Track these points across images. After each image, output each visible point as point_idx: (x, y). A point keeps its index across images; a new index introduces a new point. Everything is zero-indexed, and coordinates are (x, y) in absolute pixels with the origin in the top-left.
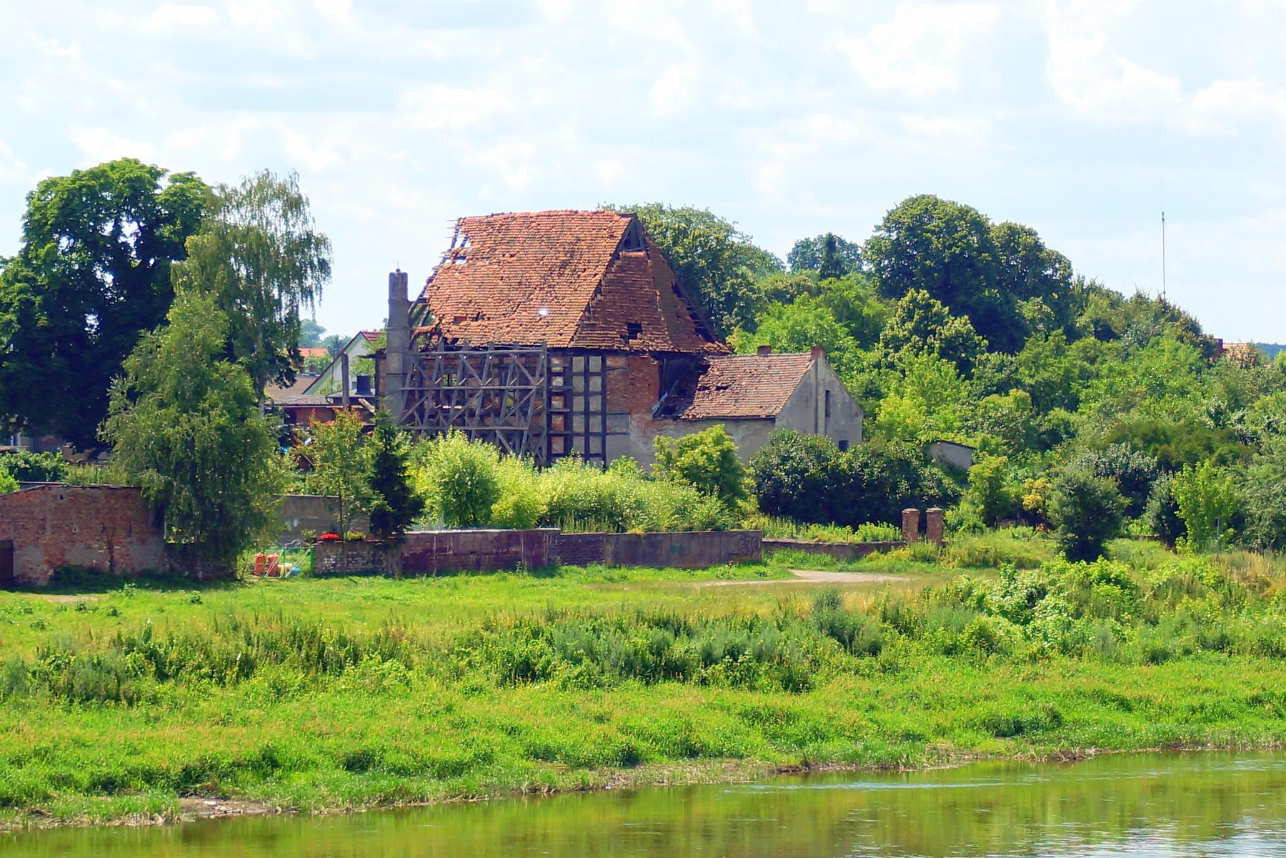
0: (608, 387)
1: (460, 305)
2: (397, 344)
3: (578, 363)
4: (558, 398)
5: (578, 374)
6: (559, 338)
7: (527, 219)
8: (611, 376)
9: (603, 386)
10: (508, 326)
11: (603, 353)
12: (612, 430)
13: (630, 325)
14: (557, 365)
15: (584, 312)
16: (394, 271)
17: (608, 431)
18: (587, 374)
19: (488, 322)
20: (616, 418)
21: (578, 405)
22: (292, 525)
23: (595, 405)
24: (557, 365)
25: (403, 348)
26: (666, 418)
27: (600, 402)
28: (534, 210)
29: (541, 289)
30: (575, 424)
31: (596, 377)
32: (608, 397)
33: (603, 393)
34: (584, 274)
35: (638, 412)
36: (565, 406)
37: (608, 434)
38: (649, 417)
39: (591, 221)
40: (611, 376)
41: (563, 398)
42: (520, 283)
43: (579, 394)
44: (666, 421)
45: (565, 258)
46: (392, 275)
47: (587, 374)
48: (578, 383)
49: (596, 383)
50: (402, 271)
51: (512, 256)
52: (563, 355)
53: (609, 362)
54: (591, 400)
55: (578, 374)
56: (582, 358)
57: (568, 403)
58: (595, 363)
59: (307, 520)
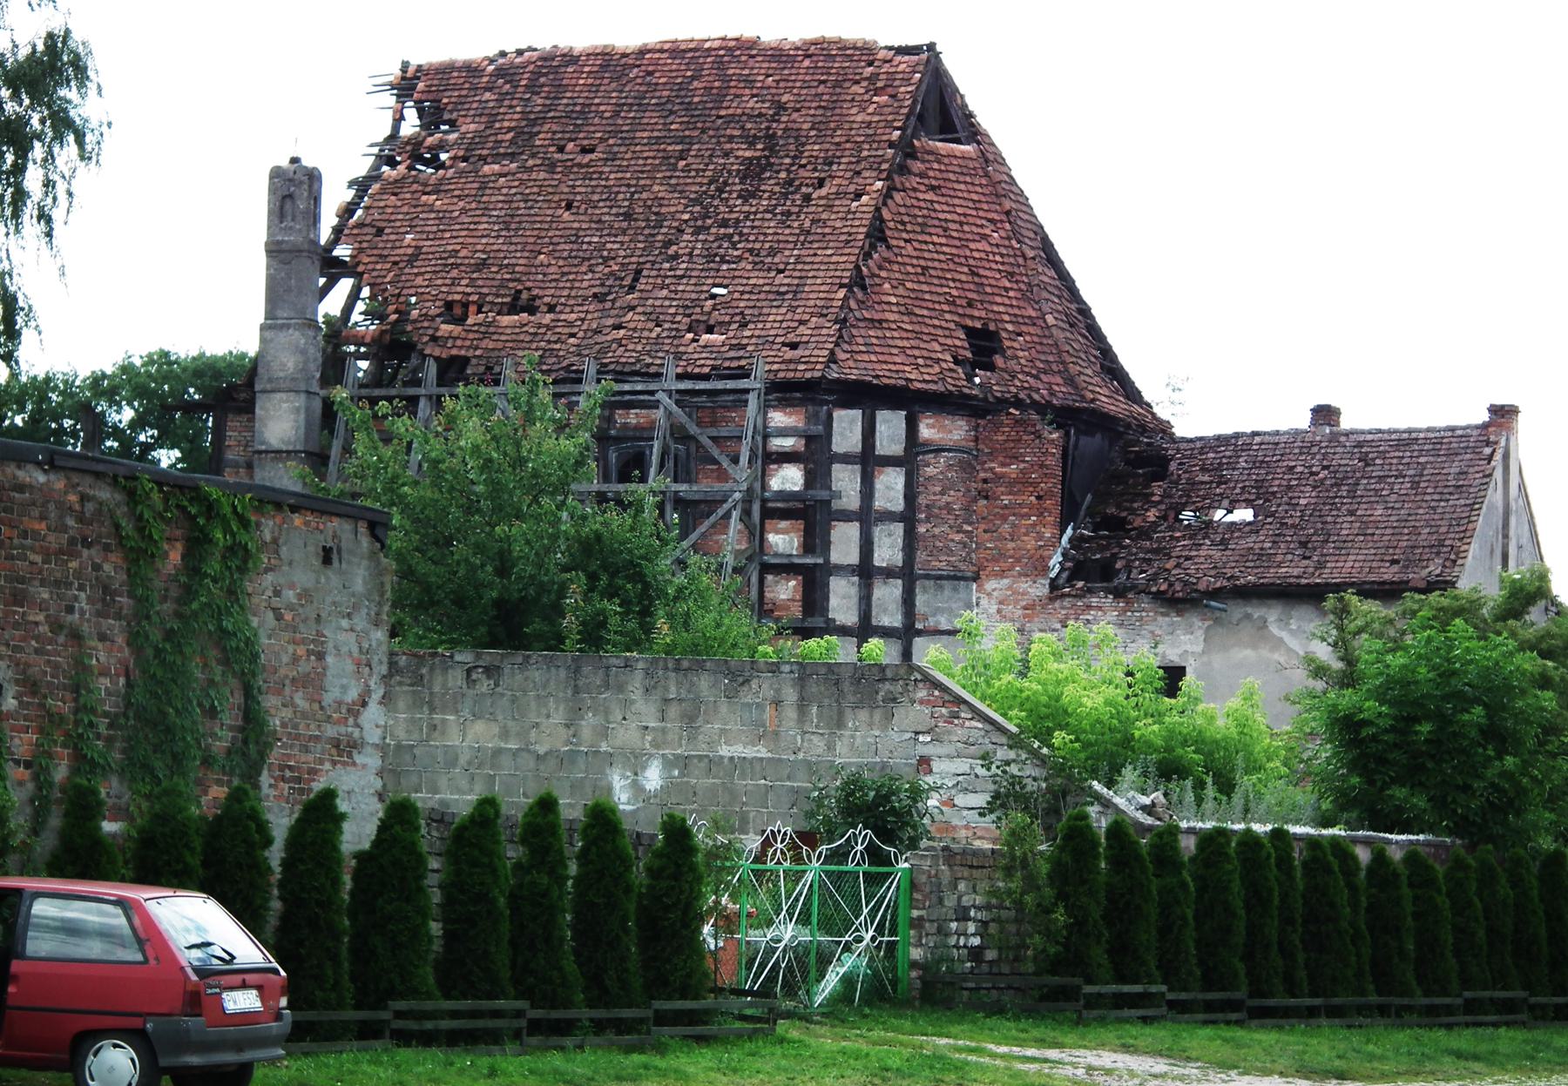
0: (922, 500)
1: (454, 273)
2: (291, 365)
3: (847, 428)
4: (784, 524)
5: (846, 459)
6: (790, 354)
7: (609, 63)
8: (930, 471)
9: (910, 495)
10: (618, 327)
11: (911, 401)
12: (931, 622)
13: (971, 333)
14: (783, 432)
15: (849, 287)
16: (284, 162)
17: (919, 626)
18: (868, 461)
19: (549, 317)
20: (941, 587)
21: (844, 544)
22: (637, 788)
23: (888, 550)
24: (783, 432)
25: (308, 380)
26: (1090, 591)
27: (900, 541)
28: (627, 38)
29: (698, 231)
30: (834, 602)
31: (890, 470)
32: (922, 529)
33: (908, 518)
34: (823, 192)
35: (1002, 574)
36: (808, 548)
37: (920, 633)
38: (1040, 589)
39: (807, 63)
40: (930, 471)
41: (800, 524)
42: (628, 216)
43: (846, 516)
44: (1094, 601)
45: (748, 154)
46: (276, 173)
47: (868, 461)
48: (846, 481)
49: (890, 487)
50: (307, 162)
51: (585, 150)
52: (802, 403)
53: (926, 431)
54: (878, 532)
55: (846, 459)
56: (857, 414)
57: (815, 539)
58: (890, 429)
59: (713, 763)
